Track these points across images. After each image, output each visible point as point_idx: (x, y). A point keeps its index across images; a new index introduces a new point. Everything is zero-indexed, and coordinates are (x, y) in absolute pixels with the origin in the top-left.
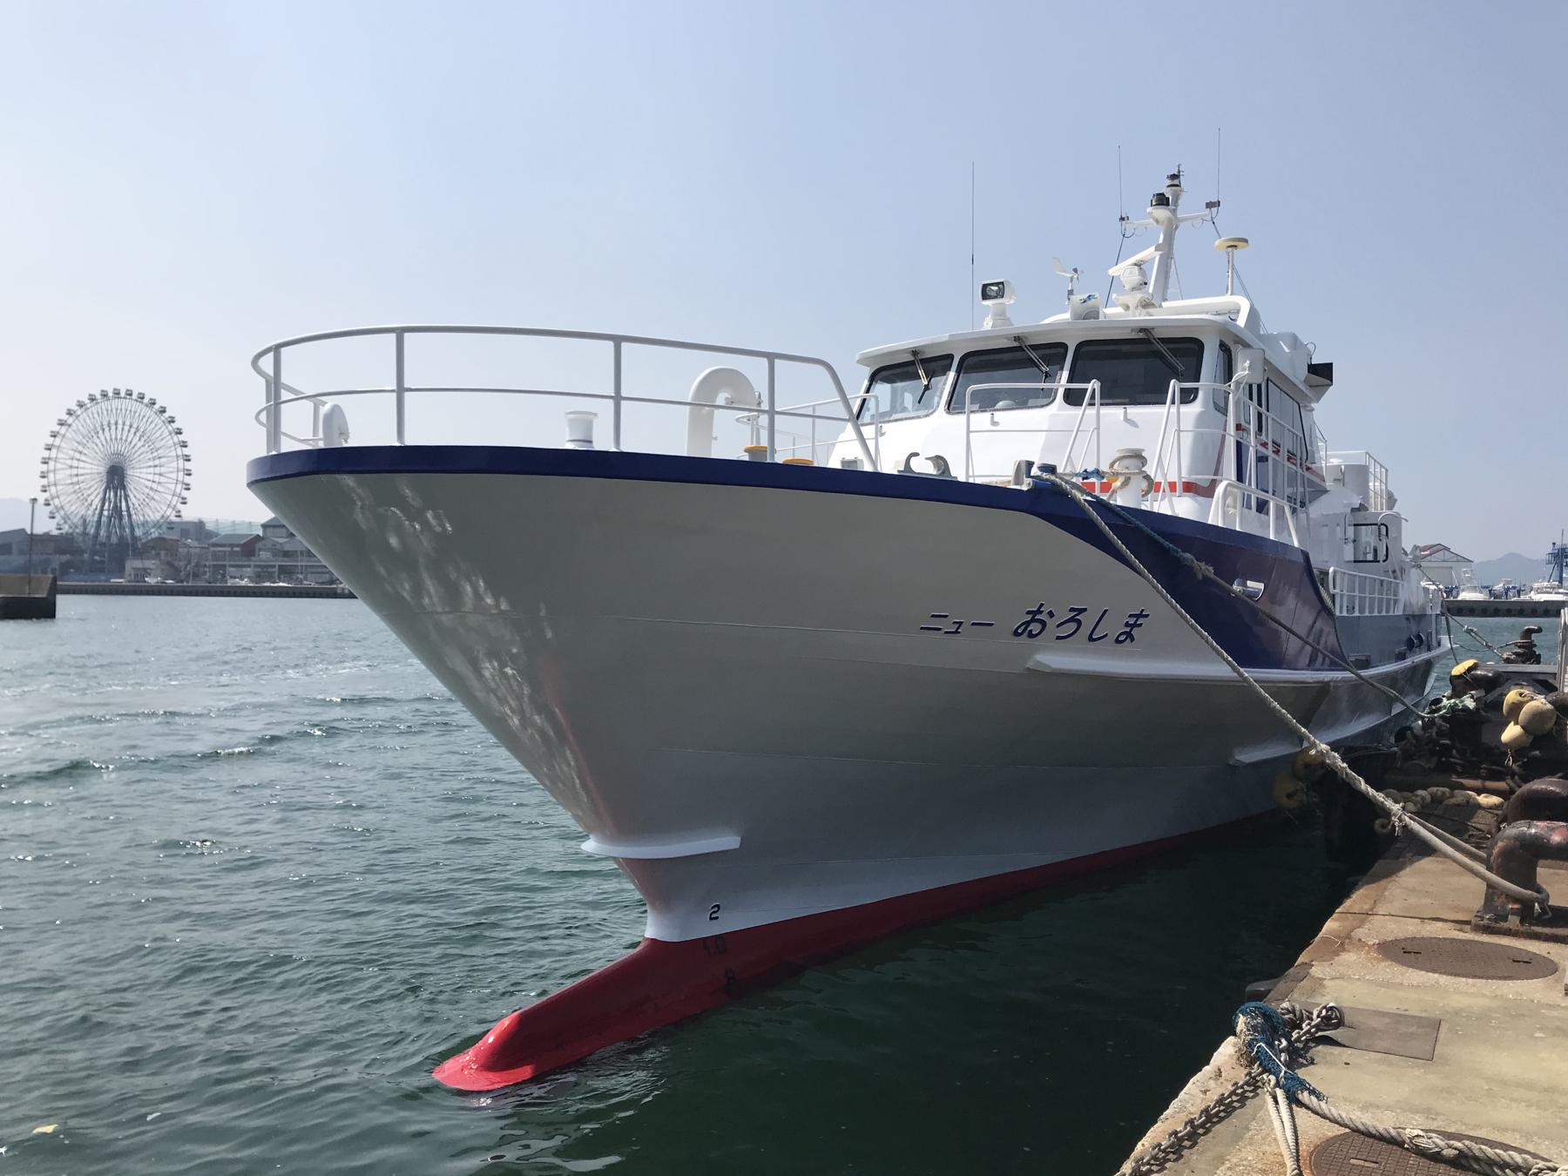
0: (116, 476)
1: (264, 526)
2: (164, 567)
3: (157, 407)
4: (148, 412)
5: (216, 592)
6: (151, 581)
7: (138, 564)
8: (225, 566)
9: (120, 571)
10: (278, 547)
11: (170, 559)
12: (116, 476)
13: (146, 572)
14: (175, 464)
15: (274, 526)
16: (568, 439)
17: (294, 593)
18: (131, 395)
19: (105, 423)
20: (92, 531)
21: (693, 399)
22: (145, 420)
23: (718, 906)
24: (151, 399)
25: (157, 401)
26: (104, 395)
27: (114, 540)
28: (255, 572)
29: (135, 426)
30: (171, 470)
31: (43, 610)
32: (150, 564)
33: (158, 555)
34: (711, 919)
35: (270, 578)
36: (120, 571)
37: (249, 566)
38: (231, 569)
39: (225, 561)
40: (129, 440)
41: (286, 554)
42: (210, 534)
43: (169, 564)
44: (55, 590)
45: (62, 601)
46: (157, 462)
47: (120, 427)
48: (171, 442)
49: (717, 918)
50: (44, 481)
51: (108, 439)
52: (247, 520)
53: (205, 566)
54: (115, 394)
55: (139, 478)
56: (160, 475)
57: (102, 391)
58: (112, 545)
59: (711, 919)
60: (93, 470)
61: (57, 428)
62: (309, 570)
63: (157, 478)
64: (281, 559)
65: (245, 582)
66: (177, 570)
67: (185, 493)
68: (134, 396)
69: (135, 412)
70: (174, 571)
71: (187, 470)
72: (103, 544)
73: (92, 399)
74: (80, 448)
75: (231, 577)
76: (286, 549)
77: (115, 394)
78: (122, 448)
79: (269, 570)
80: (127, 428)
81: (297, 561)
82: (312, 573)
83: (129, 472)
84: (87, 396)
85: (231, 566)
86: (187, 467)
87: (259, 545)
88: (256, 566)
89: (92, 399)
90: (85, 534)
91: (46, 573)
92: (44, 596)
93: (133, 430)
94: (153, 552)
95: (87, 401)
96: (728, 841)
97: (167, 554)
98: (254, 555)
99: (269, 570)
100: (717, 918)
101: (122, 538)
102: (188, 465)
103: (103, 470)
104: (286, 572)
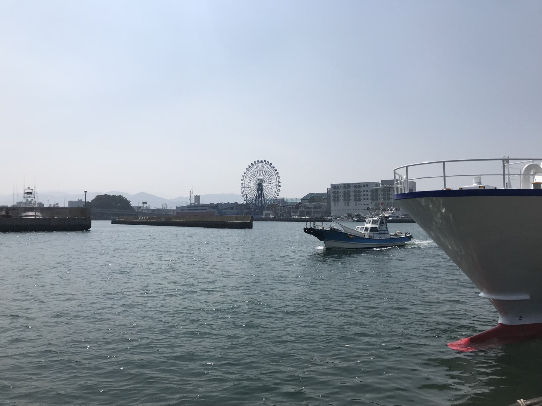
0: (260, 186)
1: (302, 199)
2: (274, 213)
3: (272, 166)
4: (267, 166)
5: (262, 220)
6: (271, 217)
7: (267, 212)
8: (291, 212)
9: (262, 214)
10: (306, 206)
11: (275, 210)
12: (260, 186)
13: (269, 214)
14: (276, 183)
15: (304, 199)
16: (474, 182)
17: (289, 220)
18: (265, 162)
19: (258, 170)
20: (254, 202)
21: (524, 173)
22: (267, 168)
23: (521, 316)
24: (268, 162)
25: (272, 164)
26: (258, 162)
27: (260, 205)
28: (299, 214)
29: (264, 170)
30: (275, 185)
31: (249, 226)
32: (270, 212)
33: (272, 209)
34: (519, 320)
35: (304, 216)
36: (262, 214)
37: (298, 212)
38: (293, 213)
39: (291, 210)
40: (263, 175)
41: (308, 208)
42: (286, 202)
43: (275, 212)
44: (252, 220)
45: (254, 224)
46: (271, 182)
47: (262, 171)
48: (275, 177)
49: (521, 320)
50: (242, 186)
51: (259, 175)
52: (296, 198)
53: (285, 212)
54: (264, 162)
55: (266, 187)
56: (272, 186)
57: (255, 162)
58: (259, 206)
59: (519, 320)
60: (254, 184)
61: (246, 171)
62: (315, 213)
63: (271, 187)
64: (307, 209)
65: (296, 217)
66: (277, 213)
67: (278, 192)
68: (266, 163)
69: (264, 166)
70: (276, 214)
71: (279, 185)
72: (257, 206)
73: (252, 164)
74: (250, 179)
75: (293, 215)
76: (308, 206)
77: (264, 162)
78: (262, 178)
79: (304, 213)
80: (264, 172)
81: (312, 210)
82: (316, 214)
83: (264, 185)
84: (251, 164)
85: (292, 212)
86: (279, 184)
87: (300, 205)
88: (299, 212)
89: (252, 164)
90: (252, 203)
91: (243, 215)
92: (250, 222)
93: (264, 172)
94: (271, 208)
95: (254, 163)
96: (526, 297)
97: (274, 209)
98: (299, 209)
99: (304, 213)
100: (521, 320)
101: (262, 204)
102: (280, 184)
103: (257, 184)
104: (309, 214)
